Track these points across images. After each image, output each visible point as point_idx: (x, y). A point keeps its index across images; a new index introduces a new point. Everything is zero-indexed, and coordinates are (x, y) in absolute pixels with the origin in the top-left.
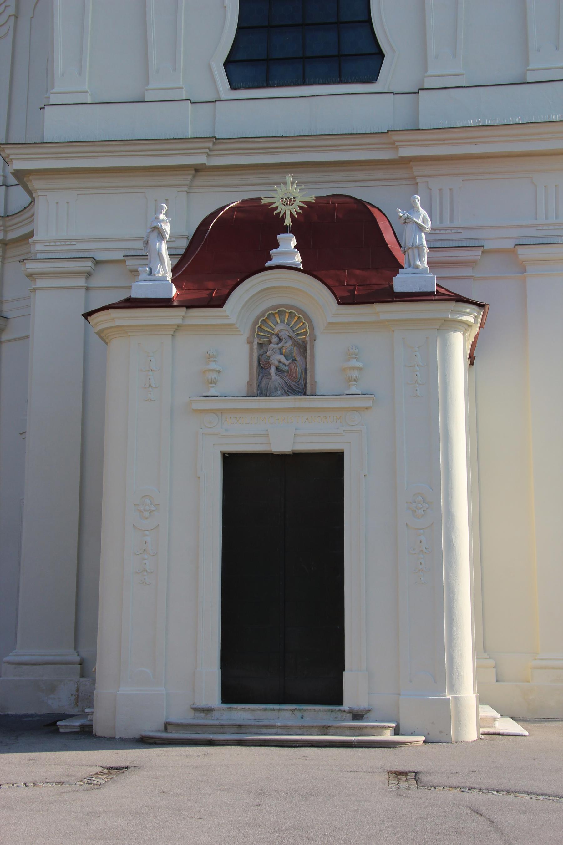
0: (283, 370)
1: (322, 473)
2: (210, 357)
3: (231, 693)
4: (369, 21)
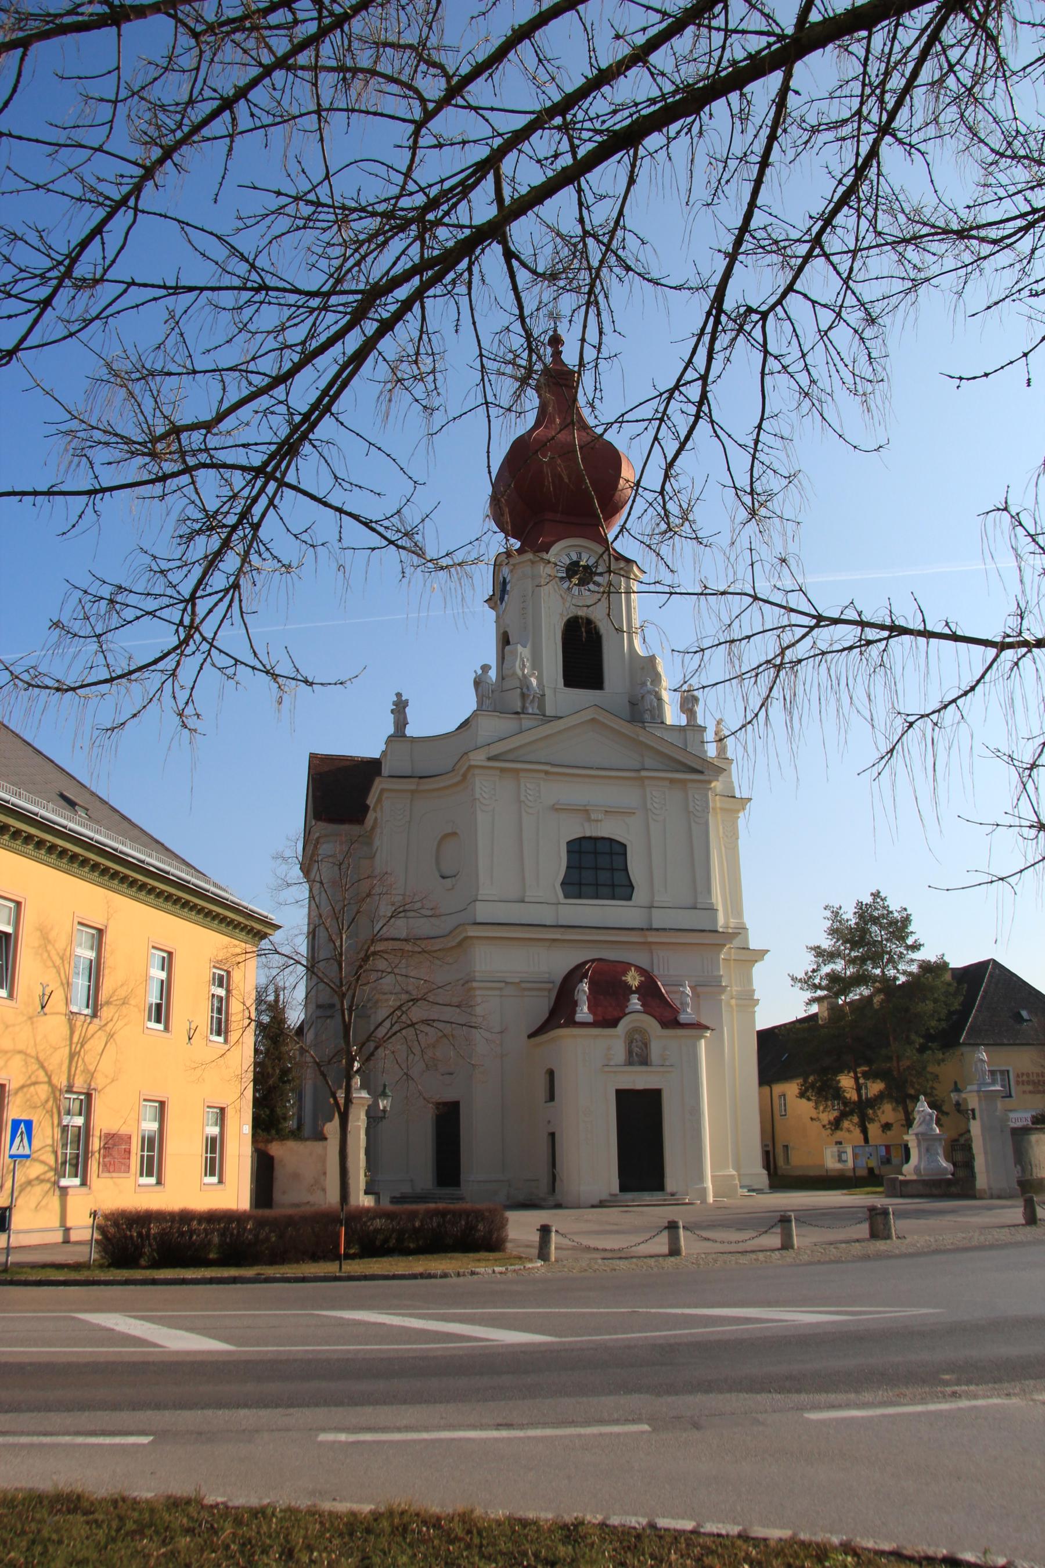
0: (638, 1055)
3: (623, 1188)
4: (626, 870)
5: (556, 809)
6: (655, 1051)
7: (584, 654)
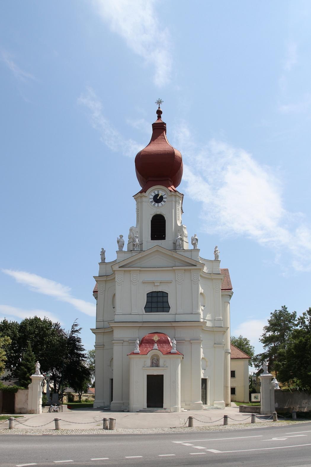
0: (155, 363)
1: (161, 377)
2: (145, 362)
3: (148, 406)
5: (144, 283)
6: (161, 363)
7: (158, 227)
